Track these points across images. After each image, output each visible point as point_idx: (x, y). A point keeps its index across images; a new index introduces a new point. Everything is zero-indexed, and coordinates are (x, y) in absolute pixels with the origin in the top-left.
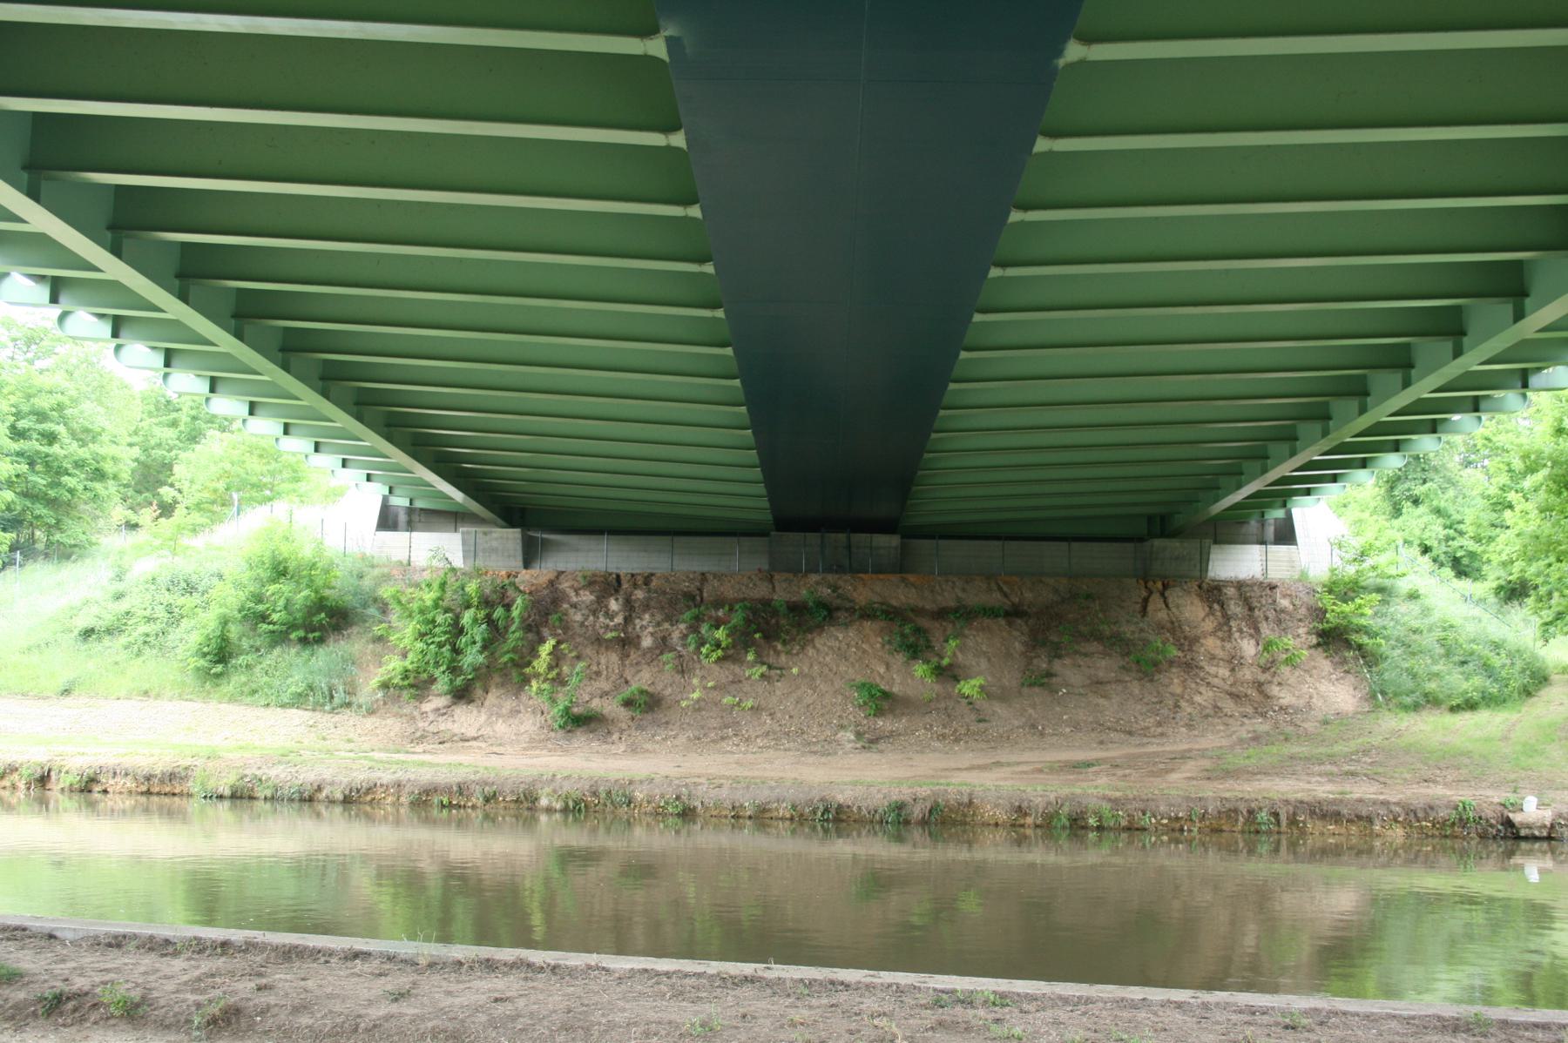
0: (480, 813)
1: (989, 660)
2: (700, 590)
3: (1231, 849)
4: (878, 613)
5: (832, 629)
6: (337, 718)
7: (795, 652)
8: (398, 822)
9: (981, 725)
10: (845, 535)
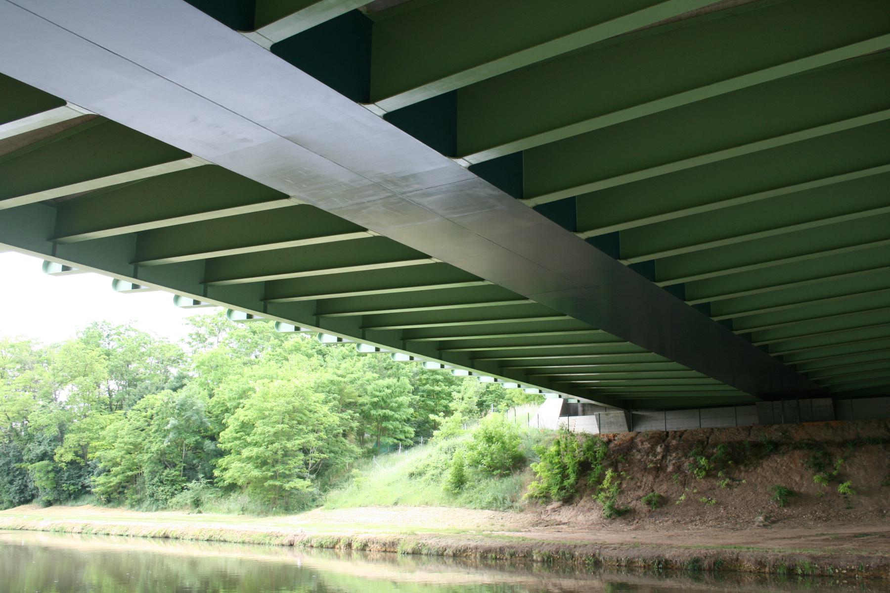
1: (866, 470)
2: (708, 438)
4: (804, 445)
5: (775, 456)
6: (505, 514)
7: (750, 470)
9: (848, 511)
10: (780, 402)
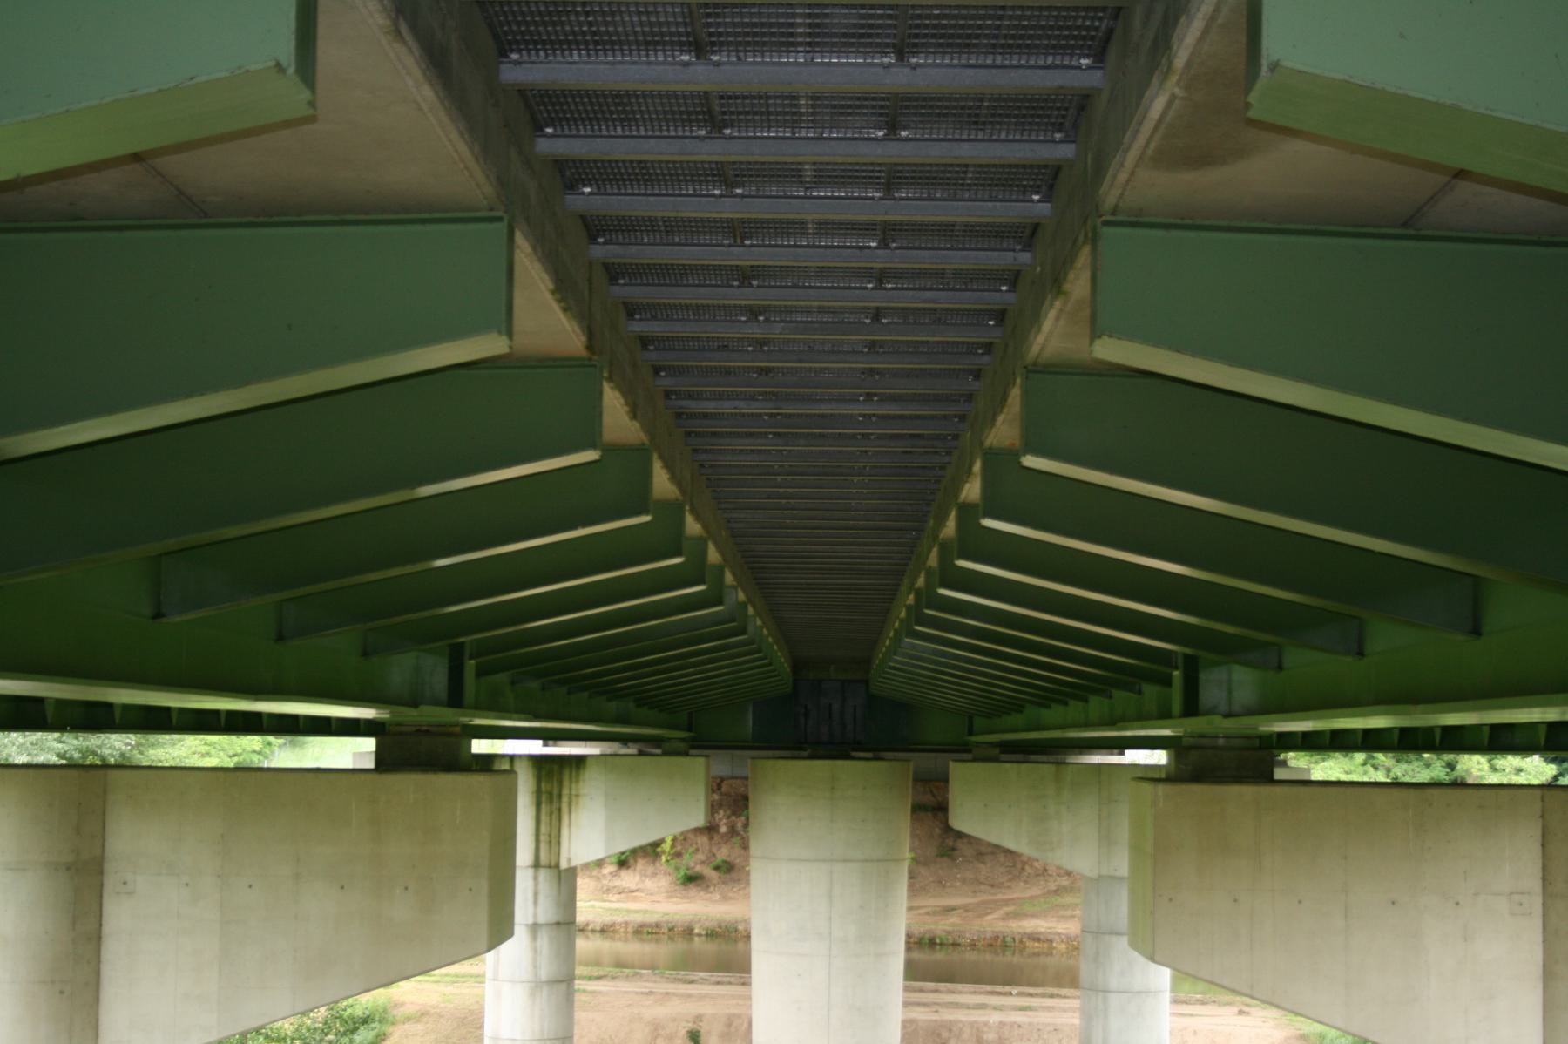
0: (666, 937)
3: (996, 953)
8: (626, 940)
